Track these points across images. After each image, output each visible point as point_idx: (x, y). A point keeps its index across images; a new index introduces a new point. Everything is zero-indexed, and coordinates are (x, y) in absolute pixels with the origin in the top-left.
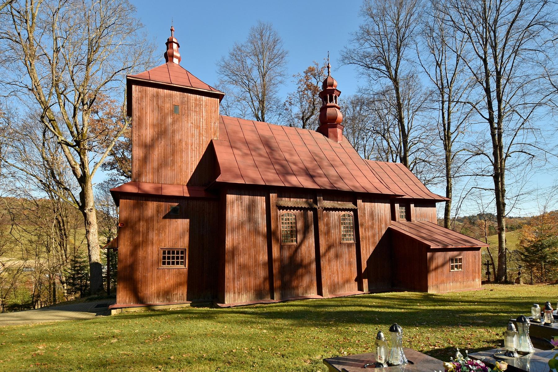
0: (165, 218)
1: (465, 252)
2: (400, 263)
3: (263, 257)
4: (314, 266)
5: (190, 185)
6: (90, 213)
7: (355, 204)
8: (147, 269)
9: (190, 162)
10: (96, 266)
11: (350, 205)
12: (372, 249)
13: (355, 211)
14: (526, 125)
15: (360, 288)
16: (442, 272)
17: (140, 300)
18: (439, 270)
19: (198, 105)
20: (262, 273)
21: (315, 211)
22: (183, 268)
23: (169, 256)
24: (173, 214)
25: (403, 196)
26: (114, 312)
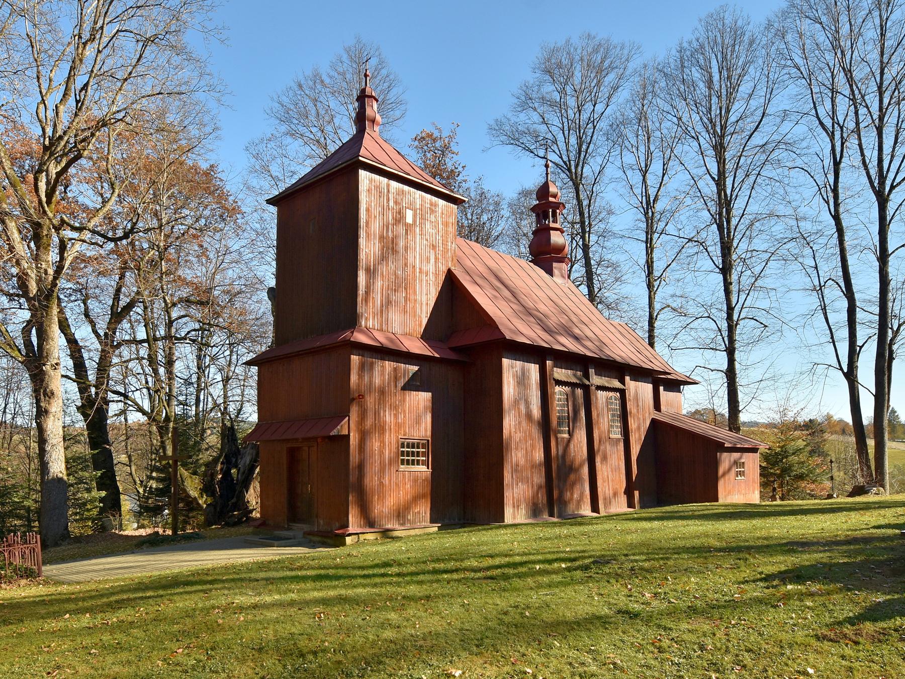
0: (404, 388)
1: (746, 455)
2: (677, 466)
3: (539, 455)
4: (585, 470)
5: (427, 336)
6: (52, 373)
7: (623, 382)
8: (382, 470)
9: (426, 296)
10: (54, 489)
11: (616, 384)
12: (638, 450)
13: (622, 392)
14: (759, 283)
15: (631, 505)
16: (729, 479)
17: (370, 523)
18: (727, 477)
19: (433, 208)
20: (539, 478)
21: (586, 389)
22: (423, 470)
23: (407, 453)
24: (412, 385)
25: (669, 374)
26: (348, 540)
